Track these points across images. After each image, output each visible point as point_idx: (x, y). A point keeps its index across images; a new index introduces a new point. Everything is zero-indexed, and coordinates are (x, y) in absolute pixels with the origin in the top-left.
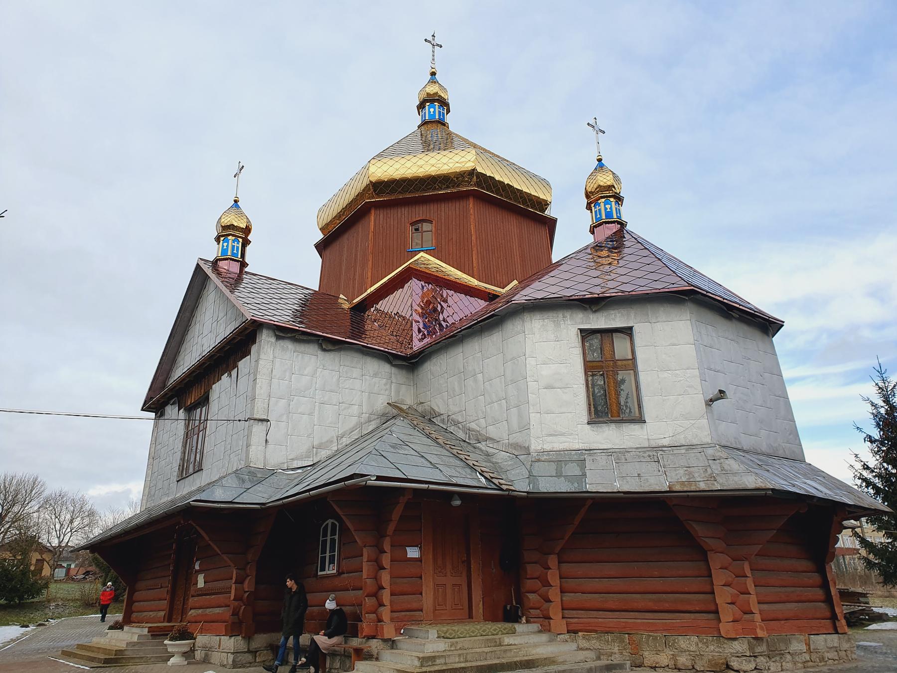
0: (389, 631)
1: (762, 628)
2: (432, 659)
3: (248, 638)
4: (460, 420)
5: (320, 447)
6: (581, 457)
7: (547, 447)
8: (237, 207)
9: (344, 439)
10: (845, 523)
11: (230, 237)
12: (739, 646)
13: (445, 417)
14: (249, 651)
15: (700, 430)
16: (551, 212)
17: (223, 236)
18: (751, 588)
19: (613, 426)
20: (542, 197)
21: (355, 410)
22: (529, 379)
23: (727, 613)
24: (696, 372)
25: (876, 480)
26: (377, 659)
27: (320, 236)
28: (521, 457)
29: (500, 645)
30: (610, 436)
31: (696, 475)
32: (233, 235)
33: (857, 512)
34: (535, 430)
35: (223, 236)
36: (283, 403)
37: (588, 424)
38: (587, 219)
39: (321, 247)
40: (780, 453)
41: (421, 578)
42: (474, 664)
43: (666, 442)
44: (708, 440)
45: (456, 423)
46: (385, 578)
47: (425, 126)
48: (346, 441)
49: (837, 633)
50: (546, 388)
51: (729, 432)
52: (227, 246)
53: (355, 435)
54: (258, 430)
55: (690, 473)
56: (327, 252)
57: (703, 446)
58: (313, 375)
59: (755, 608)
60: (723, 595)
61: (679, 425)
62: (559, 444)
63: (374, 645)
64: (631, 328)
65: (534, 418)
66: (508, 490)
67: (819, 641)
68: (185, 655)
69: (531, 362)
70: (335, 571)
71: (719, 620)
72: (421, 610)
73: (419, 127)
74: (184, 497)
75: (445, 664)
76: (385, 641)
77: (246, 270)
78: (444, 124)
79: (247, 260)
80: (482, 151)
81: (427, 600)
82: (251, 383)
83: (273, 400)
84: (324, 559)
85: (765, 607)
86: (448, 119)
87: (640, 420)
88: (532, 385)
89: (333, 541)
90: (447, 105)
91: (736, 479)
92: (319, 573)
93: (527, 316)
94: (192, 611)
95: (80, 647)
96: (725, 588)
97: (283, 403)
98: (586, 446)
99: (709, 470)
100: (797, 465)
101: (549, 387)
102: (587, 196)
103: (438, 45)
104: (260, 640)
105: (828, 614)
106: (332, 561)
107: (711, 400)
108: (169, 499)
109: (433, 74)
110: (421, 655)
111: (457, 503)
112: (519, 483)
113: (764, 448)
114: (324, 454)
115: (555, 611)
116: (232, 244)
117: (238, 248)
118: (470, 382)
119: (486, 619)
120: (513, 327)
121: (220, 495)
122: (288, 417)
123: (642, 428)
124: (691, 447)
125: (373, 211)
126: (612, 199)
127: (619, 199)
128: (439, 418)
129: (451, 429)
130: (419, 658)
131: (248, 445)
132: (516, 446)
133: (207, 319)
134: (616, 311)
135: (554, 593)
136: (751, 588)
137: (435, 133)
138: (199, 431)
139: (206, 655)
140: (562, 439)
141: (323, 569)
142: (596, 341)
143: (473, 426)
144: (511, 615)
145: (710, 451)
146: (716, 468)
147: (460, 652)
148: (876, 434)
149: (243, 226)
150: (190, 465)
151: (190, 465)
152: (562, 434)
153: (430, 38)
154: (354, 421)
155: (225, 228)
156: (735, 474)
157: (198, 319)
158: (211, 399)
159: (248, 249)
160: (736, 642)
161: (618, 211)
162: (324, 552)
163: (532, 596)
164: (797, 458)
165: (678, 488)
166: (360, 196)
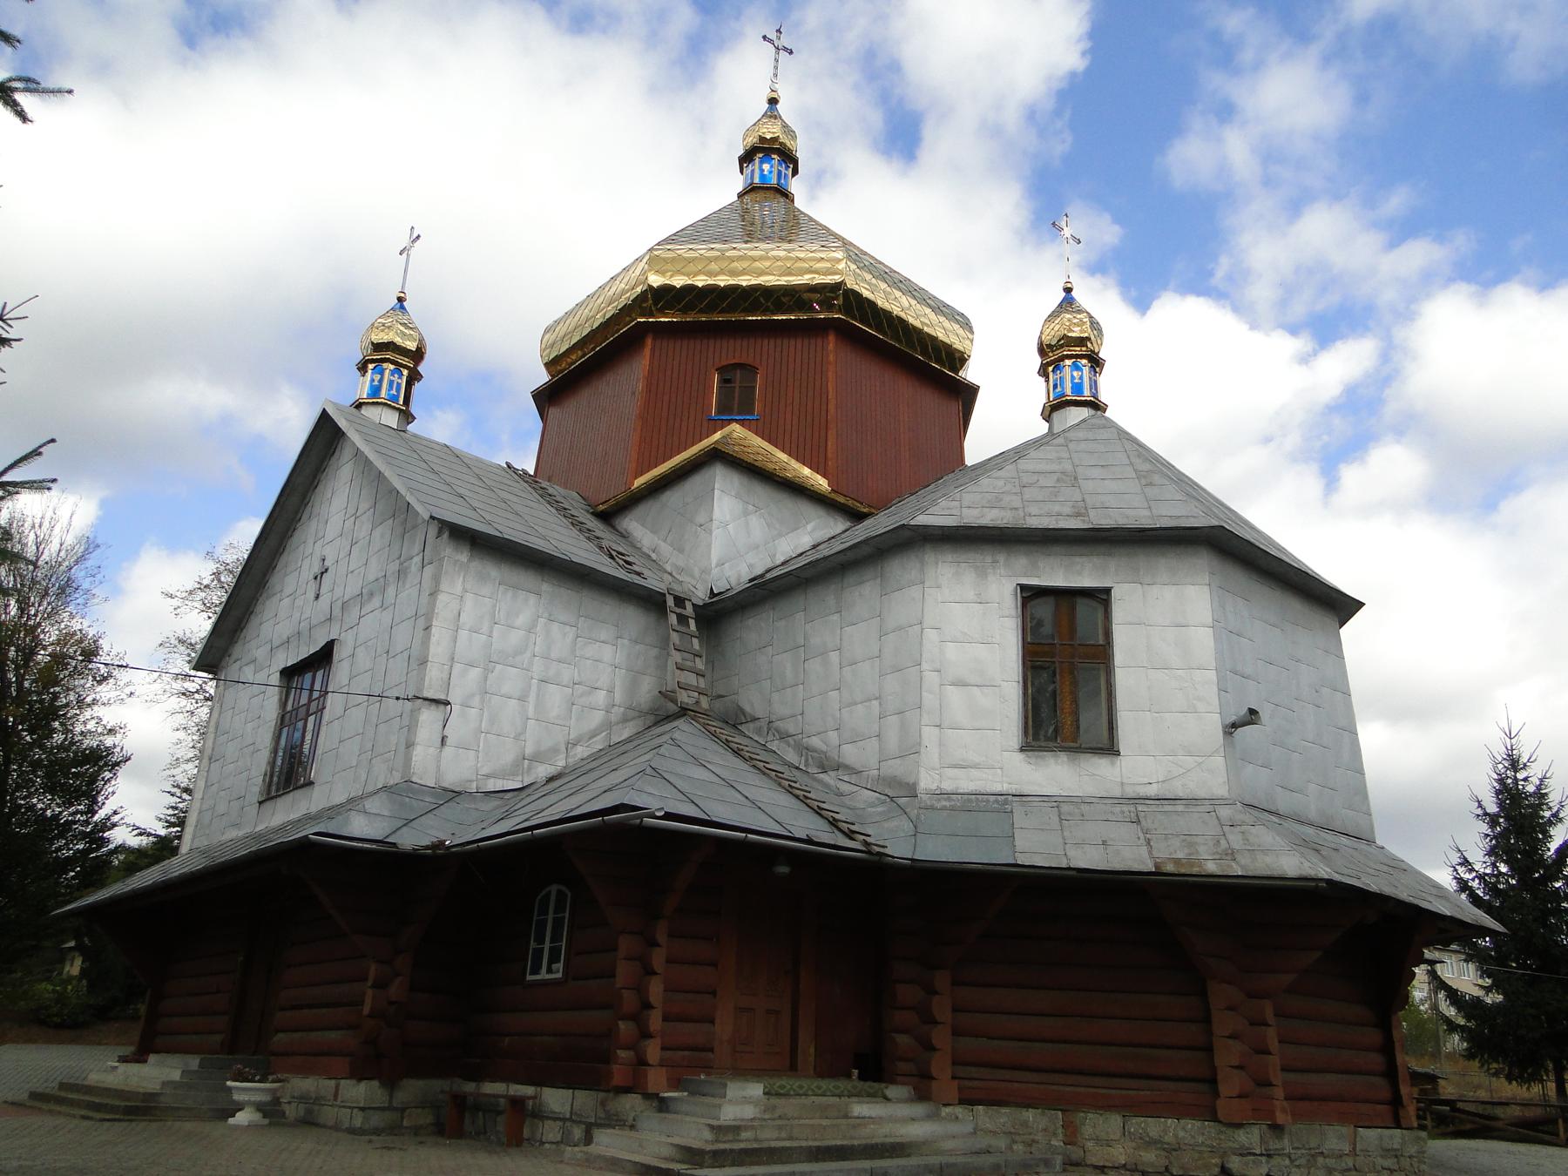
0: (656, 1079)
1: (1284, 1111)
2: (735, 1129)
3: (390, 1083)
4: (792, 730)
5: (537, 758)
6: (1004, 804)
7: (947, 786)
8: (402, 307)
9: (579, 749)
10: (1428, 954)
11: (385, 365)
12: (1250, 1137)
13: (763, 723)
14: (390, 1108)
15: (1210, 775)
16: (970, 374)
17: (372, 361)
18: (1274, 1045)
19: (1063, 756)
20: (958, 346)
21: (600, 697)
22: (925, 666)
23: (1231, 1083)
24: (1212, 675)
25: (1475, 884)
26: (632, 1127)
27: (542, 377)
28: (902, 801)
29: (846, 1117)
30: (1055, 775)
31: (1202, 849)
32: (393, 362)
33: (1449, 932)
34: (931, 754)
35: (372, 361)
36: (475, 673)
37: (1022, 750)
38: (1037, 392)
39: (545, 398)
40: (1338, 826)
41: (714, 993)
42: (804, 1144)
43: (1152, 791)
44: (1222, 791)
45: (784, 736)
46: (656, 990)
47: (753, 195)
48: (581, 752)
49: (1399, 1126)
50: (953, 684)
51: (1259, 781)
52: (381, 381)
53: (598, 744)
54: (429, 718)
55: (1191, 845)
56: (553, 412)
57: (1215, 802)
58: (530, 630)
59: (1278, 1078)
60: (1227, 1055)
61: (1169, 768)
62: (967, 782)
63: (630, 1104)
64: (1108, 591)
65: (929, 735)
66: (879, 853)
67: (1370, 1135)
68: (259, 1107)
69: (930, 635)
70: (559, 975)
71: (1216, 1094)
72: (712, 1050)
73: (740, 196)
74: (282, 828)
75: (756, 1140)
76: (647, 1096)
77: (410, 427)
78: (786, 195)
79: (414, 409)
80: (856, 255)
81: (724, 1028)
82: (420, 633)
83: (457, 668)
84: (538, 954)
85: (1292, 1076)
86: (795, 186)
87: (1109, 749)
88: (931, 678)
89: (558, 924)
90: (795, 162)
91: (1268, 860)
92: (529, 978)
93: (930, 556)
94: (281, 1035)
95: (62, 1086)
96: (1231, 1042)
97: (475, 673)
98: (1014, 789)
99: (1223, 842)
100: (1362, 846)
101: (960, 683)
102: (1043, 350)
103: (785, 49)
104: (411, 1089)
105: (1386, 1094)
106: (554, 958)
107: (1235, 726)
108: (241, 833)
109: (773, 102)
110: (715, 1123)
111: (783, 869)
112: (899, 842)
113: (1312, 814)
114: (542, 771)
115: (941, 1066)
116: (391, 379)
117: (399, 385)
118: (815, 666)
119: (821, 1074)
120: (901, 569)
121: (363, 827)
122: (482, 701)
123: (1113, 764)
124: (1192, 801)
125: (649, 341)
126: (1084, 361)
127: (1096, 363)
128: (751, 725)
129: (774, 746)
130: (712, 1127)
131: (410, 745)
132: (893, 782)
133: (333, 509)
134: (1084, 559)
135: (941, 1037)
136: (1274, 1045)
137: (769, 210)
138: (308, 715)
139: (309, 1112)
140: (974, 772)
141: (536, 971)
142: (1045, 609)
143: (815, 742)
144: (872, 1066)
145: (1224, 812)
146: (1235, 840)
147: (779, 1122)
148: (1493, 808)
149: (412, 345)
150: (290, 771)
151: (290, 771)
152: (976, 766)
153: (773, 35)
154: (597, 718)
155: (378, 347)
156: (1265, 852)
157: (316, 510)
158: (336, 657)
159: (417, 387)
160: (1241, 1132)
161: (1094, 385)
162: (541, 940)
163: (903, 1039)
164: (1364, 838)
165: (1170, 868)
166: (626, 311)
